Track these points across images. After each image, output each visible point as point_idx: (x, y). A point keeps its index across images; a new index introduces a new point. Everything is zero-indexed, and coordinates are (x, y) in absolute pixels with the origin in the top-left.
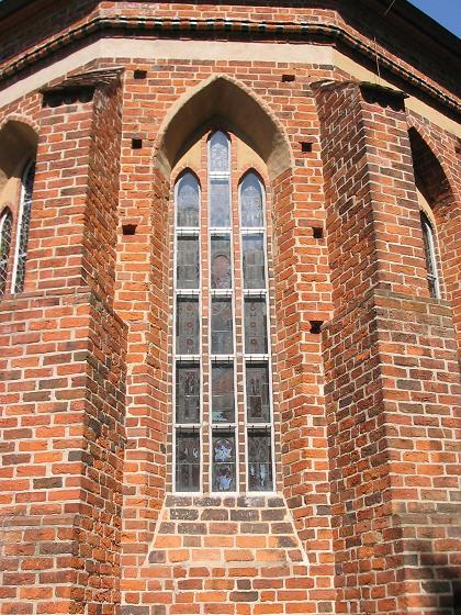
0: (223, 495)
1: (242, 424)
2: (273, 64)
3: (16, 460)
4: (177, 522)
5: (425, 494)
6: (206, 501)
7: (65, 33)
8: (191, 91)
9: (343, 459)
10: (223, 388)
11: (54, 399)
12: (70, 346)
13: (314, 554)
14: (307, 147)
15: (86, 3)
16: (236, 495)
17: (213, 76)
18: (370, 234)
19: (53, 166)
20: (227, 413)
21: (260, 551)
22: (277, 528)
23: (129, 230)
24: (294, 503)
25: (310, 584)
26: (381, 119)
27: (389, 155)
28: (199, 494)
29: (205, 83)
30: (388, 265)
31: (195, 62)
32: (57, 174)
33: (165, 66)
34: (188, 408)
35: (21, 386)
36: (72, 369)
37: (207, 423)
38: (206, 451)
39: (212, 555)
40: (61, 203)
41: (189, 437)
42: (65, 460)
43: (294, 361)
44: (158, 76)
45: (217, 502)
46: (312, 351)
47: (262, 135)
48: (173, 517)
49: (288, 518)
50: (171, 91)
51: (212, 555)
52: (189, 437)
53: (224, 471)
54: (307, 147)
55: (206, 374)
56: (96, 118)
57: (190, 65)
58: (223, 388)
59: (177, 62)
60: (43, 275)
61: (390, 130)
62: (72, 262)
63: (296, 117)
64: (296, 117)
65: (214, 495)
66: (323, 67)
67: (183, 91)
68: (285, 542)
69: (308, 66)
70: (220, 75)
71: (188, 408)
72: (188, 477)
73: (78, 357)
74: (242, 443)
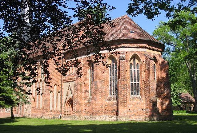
0: (135, 95)
1: (137, 89)
6: (134, 96)
7: (118, 46)
9: (146, 93)
10: (135, 85)
13: (143, 101)
14: (143, 62)
15: (1, 49)
16: (136, 95)
18: (149, 74)
20: (135, 88)
21: (139, 100)
23: (127, 71)
24: (141, 96)
29: (133, 54)
30: (151, 77)
34: (132, 87)
37: (133, 89)
38: (133, 91)
39: (135, 101)
41: (132, 90)
43: (142, 84)
46: (143, 83)
47: (139, 60)
49: (141, 98)
51: (135, 101)
52: (132, 90)
53: (135, 93)
54: (143, 62)
55: (133, 84)
56: (179, 10)
58: (135, 85)
63: (142, 58)
64: (142, 58)
71: (132, 87)
72: (132, 94)
74: (137, 91)
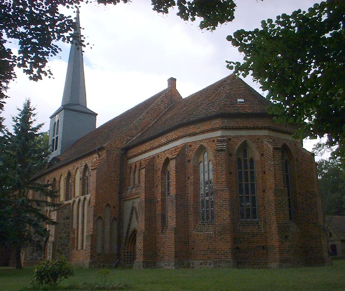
2: (256, 136)
3: (219, 216)
4: (241, 225)
5: (282, 221)
8: (240, 143)
11: (224, 207)
12: (226, 198)
16: (251, 220)
17: (244, 139)
19: (219, 165)
22: (258, 226)
25: (263, 234)
26: (277, 154)
27: (277, 161)
28: (244, 220)
31: (241, 136)
32: (220, 167)
33: (234, 137)
35: (219, 205)
36: (227, 202)
40: (221, 173)
42: (227, 216)
44: (233, 139)
45: (247, 221)
48: (241, 224)
50: (236, 143)
57: (239, 137)
59: (237, 136)
60: (220, 186)
61: (278, 156)
62: (224, 184)
65: (247, 220)
66: (266, 136)
67: (238, 143)
68: (259, 228)
69: (263, 136)
70: (245, 139)
73: (228, 200)
